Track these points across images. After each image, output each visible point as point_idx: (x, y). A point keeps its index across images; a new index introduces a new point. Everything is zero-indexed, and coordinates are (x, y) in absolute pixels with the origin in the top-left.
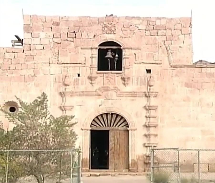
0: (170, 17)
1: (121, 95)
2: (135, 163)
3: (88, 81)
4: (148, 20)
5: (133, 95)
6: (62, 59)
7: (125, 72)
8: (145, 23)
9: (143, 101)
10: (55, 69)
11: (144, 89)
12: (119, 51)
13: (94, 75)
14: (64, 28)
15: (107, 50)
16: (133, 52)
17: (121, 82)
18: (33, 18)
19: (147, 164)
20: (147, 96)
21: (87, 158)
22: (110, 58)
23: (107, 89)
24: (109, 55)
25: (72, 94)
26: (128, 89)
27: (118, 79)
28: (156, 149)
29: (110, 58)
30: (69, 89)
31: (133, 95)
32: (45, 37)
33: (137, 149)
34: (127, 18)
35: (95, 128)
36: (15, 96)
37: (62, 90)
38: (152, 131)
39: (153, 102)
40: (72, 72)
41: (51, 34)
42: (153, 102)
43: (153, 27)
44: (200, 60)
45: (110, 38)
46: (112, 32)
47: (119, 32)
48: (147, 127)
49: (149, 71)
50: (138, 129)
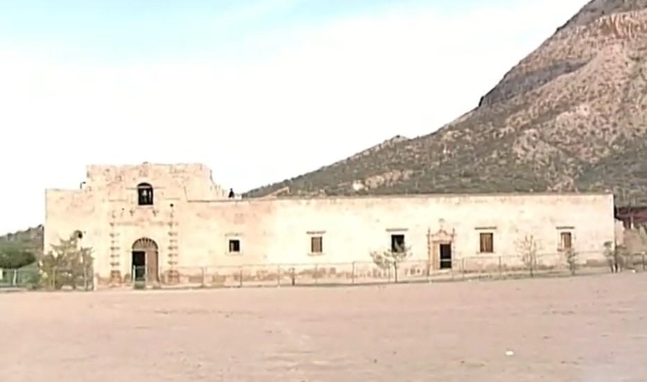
0: (186, 162)
1: (152, 224)
2: (163, 277)
3: (129, 214)
4: (171, 166)
5: (161, 224)
6: (112, 198)
7: (155, 206)
8: (168, 168)
9: (168, 229)
10: (107, 206)
11: (169, 220)
12: (150, 190)
13: (134, 209)
14: (113, 174)
15: (143, 190)
16: (162, 190)
17: (153, 214)
18: (93, 167)
19: (170, 277)
20: (170, 224)
21: (643, 259)
22: (145, 196)
23: (142, 220)
24: (145, 193)
25: (119, 224)
26: (159, 218)
27: (150, 211)
28: (616, 243)
29: (145, 196)
30: (117, 220)
31: (161, 224)
32: (100, 180)
33: (164, 265)
34: (157, 165)
35: (136, 250)
36: (211, 171)
37: (112, 220)
38: (174, 251)
39: (174, 229)
40: (118, 207)
41: (104, 178)
42: (174, 229)
43: (174, 171)
44: (397, 134)
45: (144, 180)
46: (145, 175)
47: (151, 175)
48: (170, 248)
49: (172, 205)
50: (306, 231)
